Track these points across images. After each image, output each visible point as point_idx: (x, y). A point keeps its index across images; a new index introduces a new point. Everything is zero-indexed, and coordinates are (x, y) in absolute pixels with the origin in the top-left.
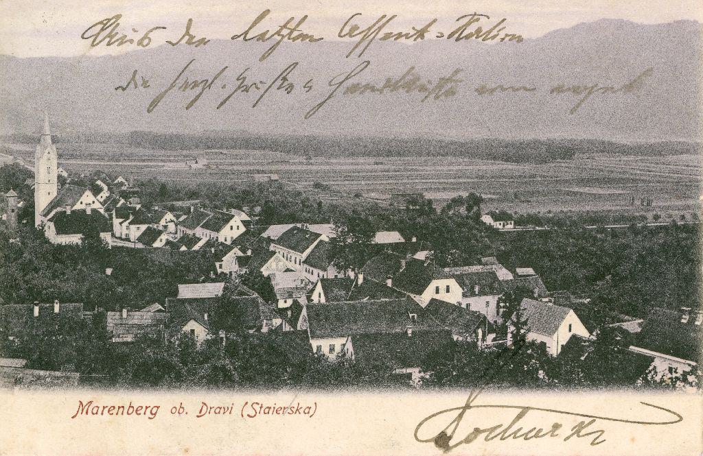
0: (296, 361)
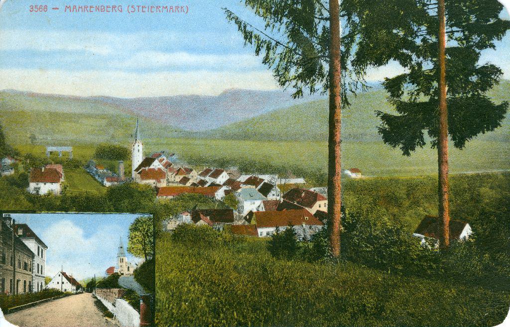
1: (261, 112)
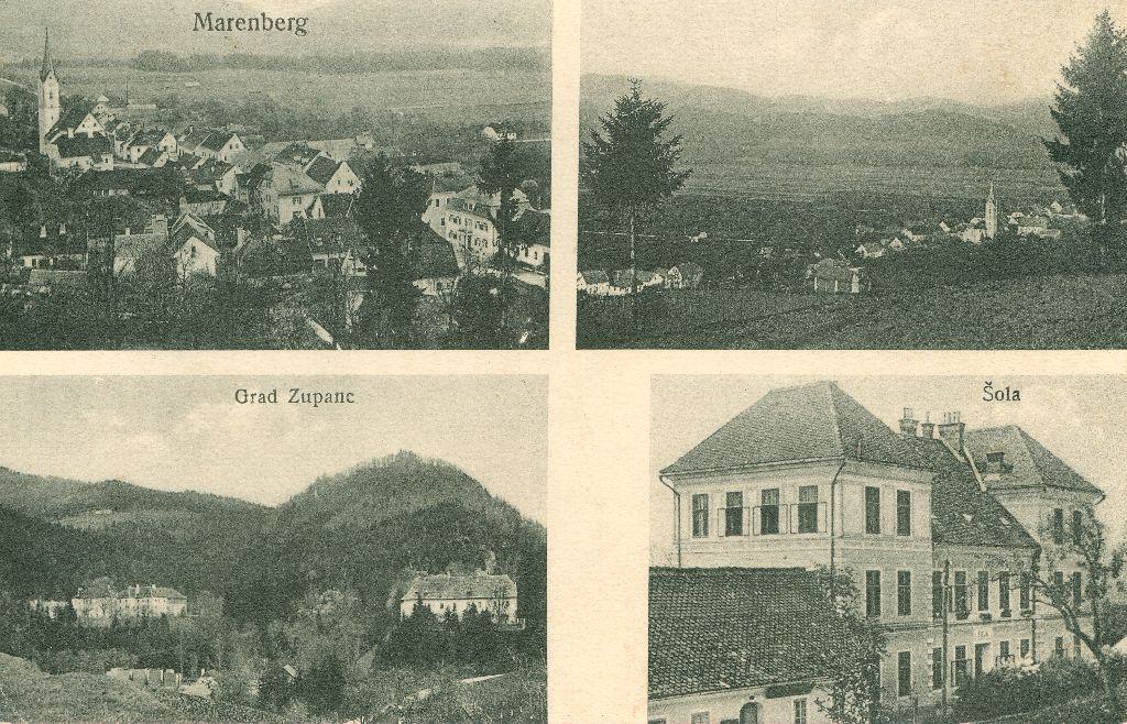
0: (914, 695)
1: (463, 43)
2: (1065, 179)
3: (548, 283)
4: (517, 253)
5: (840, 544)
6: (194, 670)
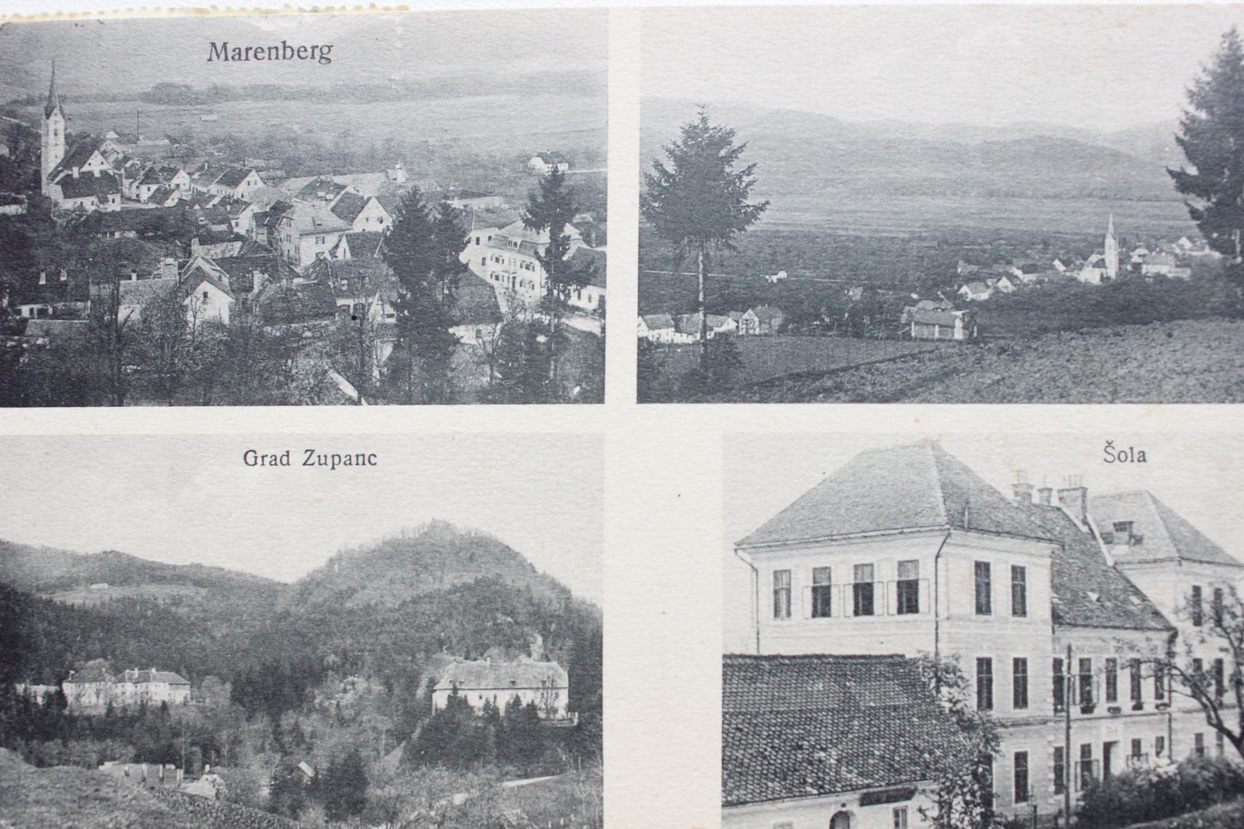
2: (1195, 214)
3: (603, 329)
4: (568, 296)
5: (945, 628)
6: (196, 766)
